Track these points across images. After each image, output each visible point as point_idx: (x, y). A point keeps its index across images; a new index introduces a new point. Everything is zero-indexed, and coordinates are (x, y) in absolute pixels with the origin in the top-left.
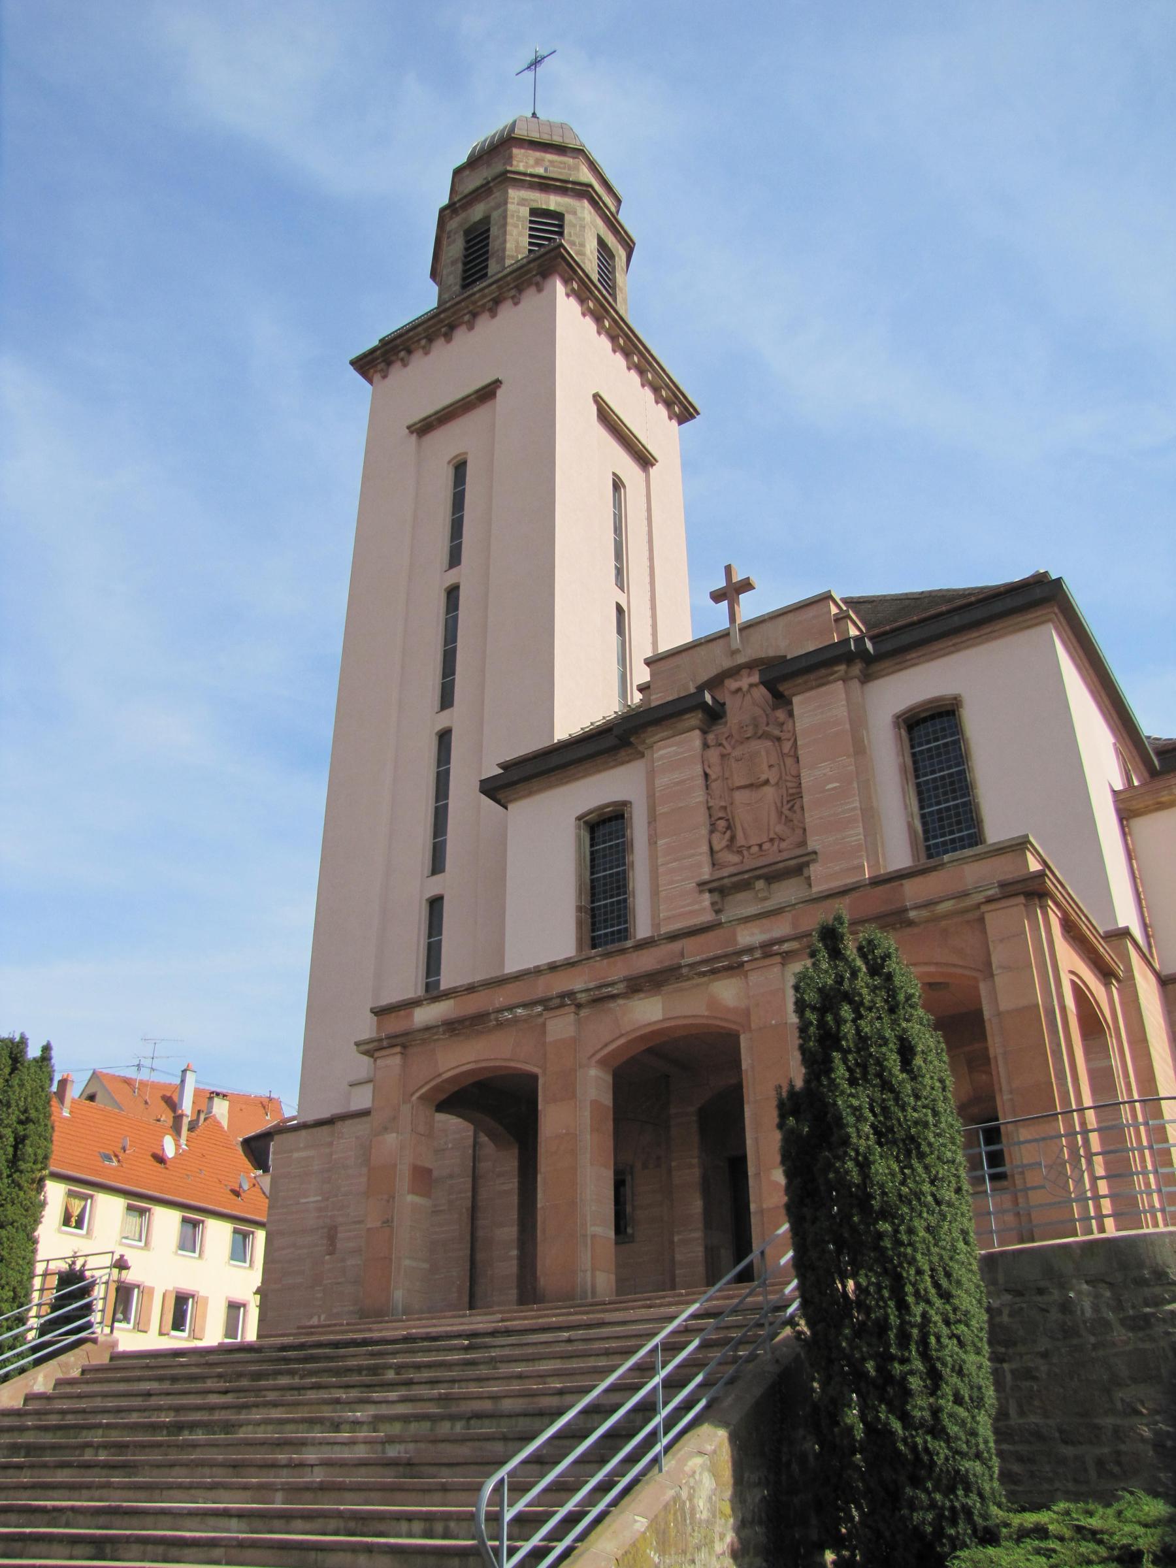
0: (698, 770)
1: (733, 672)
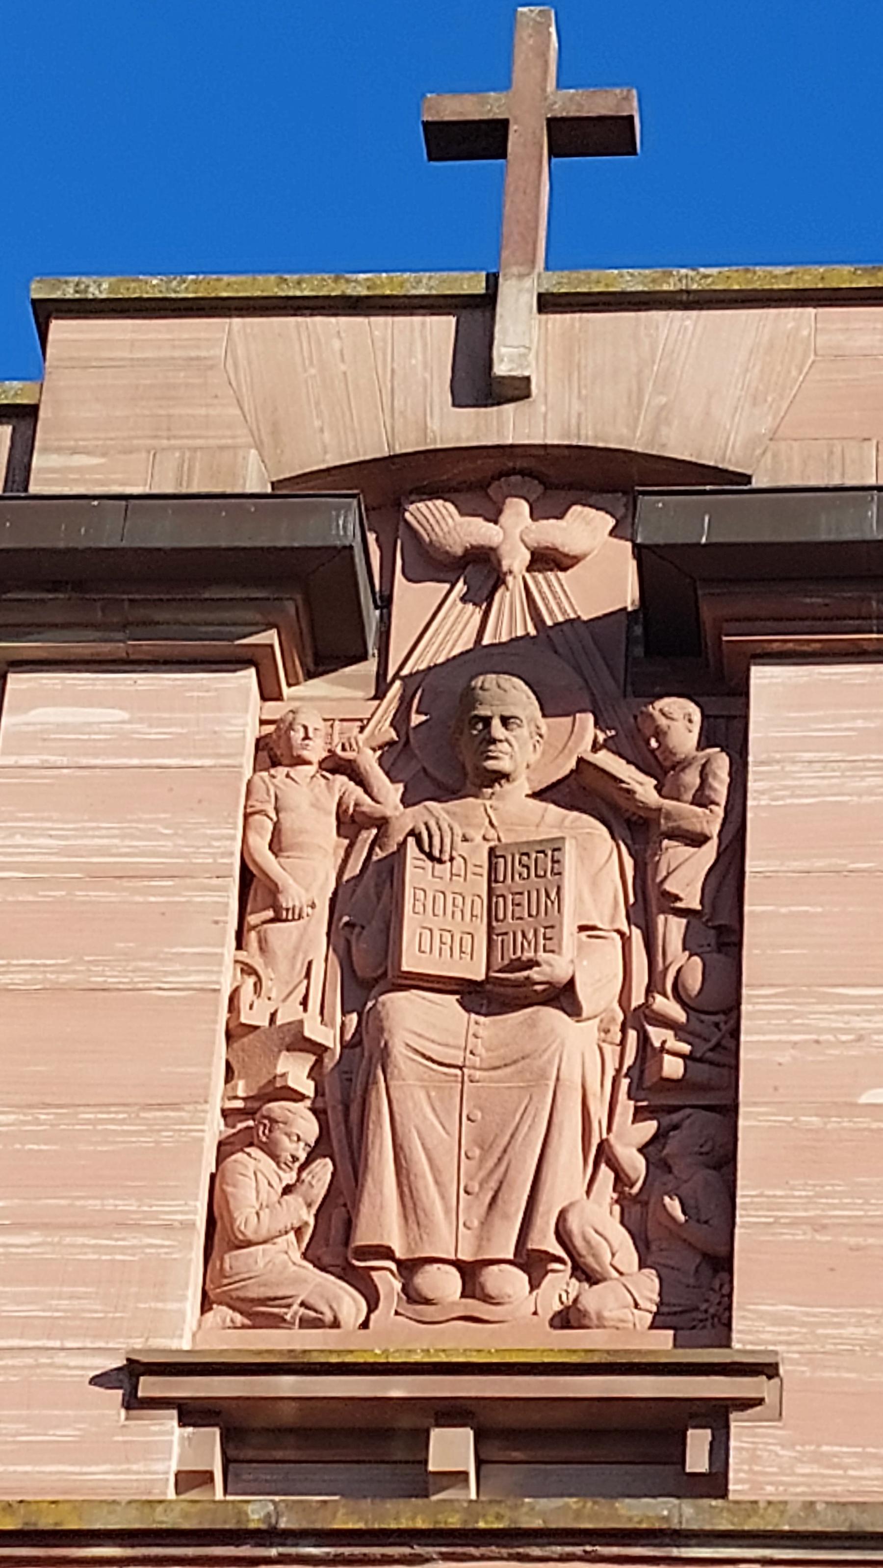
0: (221, 847)
1: (479, 477)
